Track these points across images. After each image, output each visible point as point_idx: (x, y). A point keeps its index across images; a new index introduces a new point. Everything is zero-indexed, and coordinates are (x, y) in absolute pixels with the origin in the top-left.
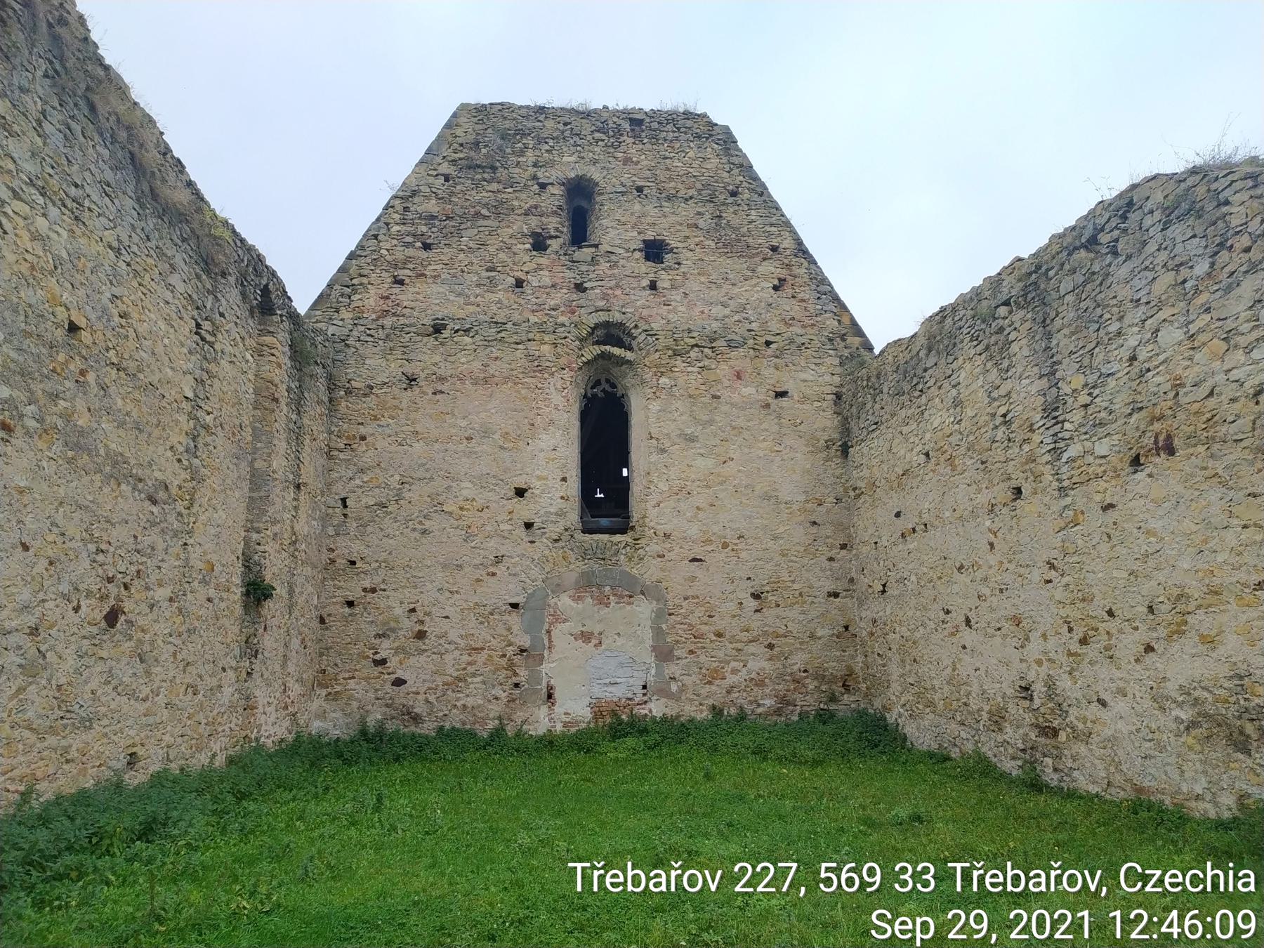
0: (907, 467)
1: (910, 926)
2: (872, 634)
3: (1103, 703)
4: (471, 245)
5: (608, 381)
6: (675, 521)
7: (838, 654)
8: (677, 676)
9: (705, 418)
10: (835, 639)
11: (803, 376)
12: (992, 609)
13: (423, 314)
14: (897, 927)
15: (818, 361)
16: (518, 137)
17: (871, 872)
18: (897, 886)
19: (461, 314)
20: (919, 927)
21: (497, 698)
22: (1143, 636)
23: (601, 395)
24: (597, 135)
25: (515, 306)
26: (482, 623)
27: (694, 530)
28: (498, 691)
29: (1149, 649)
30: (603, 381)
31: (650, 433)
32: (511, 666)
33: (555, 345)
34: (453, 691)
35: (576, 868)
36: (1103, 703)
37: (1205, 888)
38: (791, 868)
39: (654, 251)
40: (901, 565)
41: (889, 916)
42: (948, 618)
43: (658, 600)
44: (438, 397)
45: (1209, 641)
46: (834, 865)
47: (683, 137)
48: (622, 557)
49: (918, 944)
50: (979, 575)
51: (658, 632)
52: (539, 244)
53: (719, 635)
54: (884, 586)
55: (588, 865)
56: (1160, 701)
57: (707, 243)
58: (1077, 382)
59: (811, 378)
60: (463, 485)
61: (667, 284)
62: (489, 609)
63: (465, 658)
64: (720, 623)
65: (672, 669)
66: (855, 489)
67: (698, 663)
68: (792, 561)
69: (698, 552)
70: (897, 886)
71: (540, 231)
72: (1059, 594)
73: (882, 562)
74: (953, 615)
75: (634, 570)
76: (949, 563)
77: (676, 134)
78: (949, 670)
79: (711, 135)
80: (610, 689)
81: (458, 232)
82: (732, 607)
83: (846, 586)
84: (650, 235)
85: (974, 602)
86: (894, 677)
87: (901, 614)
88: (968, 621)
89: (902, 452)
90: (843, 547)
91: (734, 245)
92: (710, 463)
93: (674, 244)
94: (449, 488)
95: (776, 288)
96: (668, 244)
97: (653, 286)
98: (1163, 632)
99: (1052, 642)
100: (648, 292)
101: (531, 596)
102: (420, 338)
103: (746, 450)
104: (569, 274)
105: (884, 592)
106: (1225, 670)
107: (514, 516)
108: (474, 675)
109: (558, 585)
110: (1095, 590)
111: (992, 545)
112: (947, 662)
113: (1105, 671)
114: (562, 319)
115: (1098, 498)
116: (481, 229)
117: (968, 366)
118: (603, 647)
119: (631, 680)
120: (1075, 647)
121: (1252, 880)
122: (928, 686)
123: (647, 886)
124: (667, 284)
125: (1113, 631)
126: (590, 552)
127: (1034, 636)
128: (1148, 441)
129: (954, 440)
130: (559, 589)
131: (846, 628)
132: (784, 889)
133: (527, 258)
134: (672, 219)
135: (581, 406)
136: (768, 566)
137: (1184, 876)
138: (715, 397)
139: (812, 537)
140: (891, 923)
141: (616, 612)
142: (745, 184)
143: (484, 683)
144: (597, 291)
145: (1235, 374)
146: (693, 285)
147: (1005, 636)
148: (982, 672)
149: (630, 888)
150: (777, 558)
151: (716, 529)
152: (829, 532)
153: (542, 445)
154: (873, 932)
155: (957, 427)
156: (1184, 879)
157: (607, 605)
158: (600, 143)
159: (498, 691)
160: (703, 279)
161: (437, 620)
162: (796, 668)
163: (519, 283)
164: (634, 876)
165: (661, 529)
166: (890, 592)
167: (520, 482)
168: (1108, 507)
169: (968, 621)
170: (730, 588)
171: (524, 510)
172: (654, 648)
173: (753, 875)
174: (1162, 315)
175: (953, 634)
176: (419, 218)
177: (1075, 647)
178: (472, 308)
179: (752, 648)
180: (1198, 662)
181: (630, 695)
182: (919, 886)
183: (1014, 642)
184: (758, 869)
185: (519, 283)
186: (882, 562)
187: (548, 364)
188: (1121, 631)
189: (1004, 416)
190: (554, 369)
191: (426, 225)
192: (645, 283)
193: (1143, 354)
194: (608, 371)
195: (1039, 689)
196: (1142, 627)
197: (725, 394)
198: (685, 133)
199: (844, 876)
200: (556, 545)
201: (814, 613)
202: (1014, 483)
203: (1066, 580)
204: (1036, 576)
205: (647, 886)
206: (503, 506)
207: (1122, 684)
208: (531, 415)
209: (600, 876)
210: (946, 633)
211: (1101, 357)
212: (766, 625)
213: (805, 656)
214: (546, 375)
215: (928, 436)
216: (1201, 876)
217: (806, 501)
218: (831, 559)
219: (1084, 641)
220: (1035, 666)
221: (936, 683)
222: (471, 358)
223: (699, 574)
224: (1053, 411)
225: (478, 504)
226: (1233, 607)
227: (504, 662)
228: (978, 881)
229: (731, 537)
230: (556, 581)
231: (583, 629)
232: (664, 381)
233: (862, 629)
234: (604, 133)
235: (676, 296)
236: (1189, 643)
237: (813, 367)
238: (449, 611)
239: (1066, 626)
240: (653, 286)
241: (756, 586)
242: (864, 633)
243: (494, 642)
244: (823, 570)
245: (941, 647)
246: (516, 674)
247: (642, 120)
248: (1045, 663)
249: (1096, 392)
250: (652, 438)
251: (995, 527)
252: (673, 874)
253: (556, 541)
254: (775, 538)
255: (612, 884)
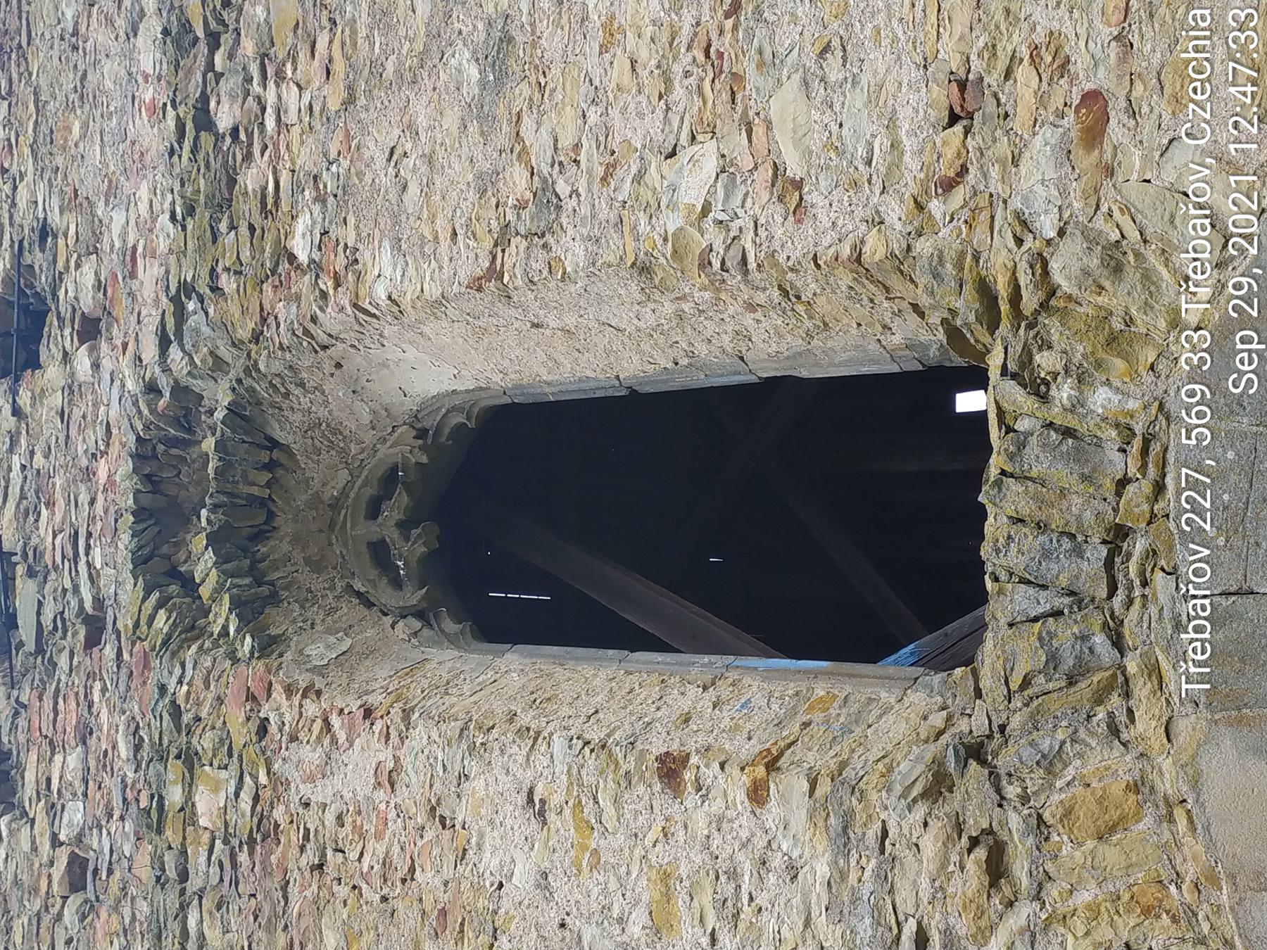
1: (1245, 355)
14: (1246, 368)
17: (1191, 394)
18: (1205, 368)
20: (1246, 347)
30: (372, 531)
31: (477, 285)
35: (1187, 690)
37: (1206, 59)
41: (1235, 376)
46: (1183, 431)
48: (1101, 398)
49: (1263, 347)
55: (1183, 677)
70: (1205, 368)
121: (1199, 12)
123: (1205, 618)
126: (1065, 632)
132: (1208, 481)
137: (1196, 80)
140: (1241, 374)
149: (1207, 635)
154: (1251, 392)
156: (1199, 80)
173: (1193, 512)
182: (1205, 346)
184: (1188, 507)
194: (335, 505)
199: (1195, 421)
200: (1020, 868)
205: (1205, 618)
209: (1195, 666)
216: (1194, 63)
228: (1200, 667)
250: (494, 273)
252: (1192, 212)
253: (996, 870)
255: (1203, 654)
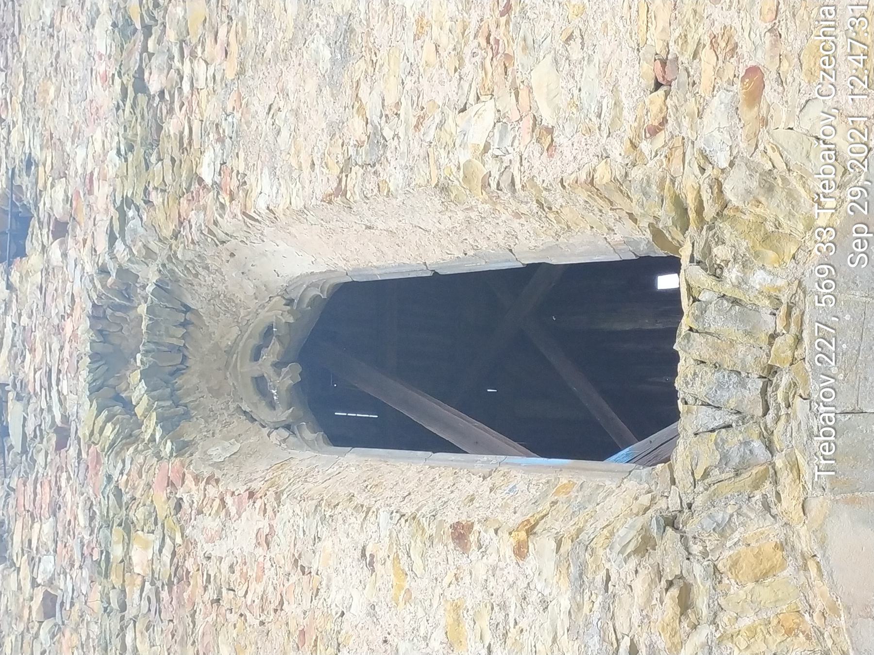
30: (256, 369)
31: (328, 199)
38: (818, 327)
48: (759, 278)
126: (733, 439)
135: (310, 445)
164: (825, 436)
194: (229, 352)
250: (340, 191)
253: (685, 603)
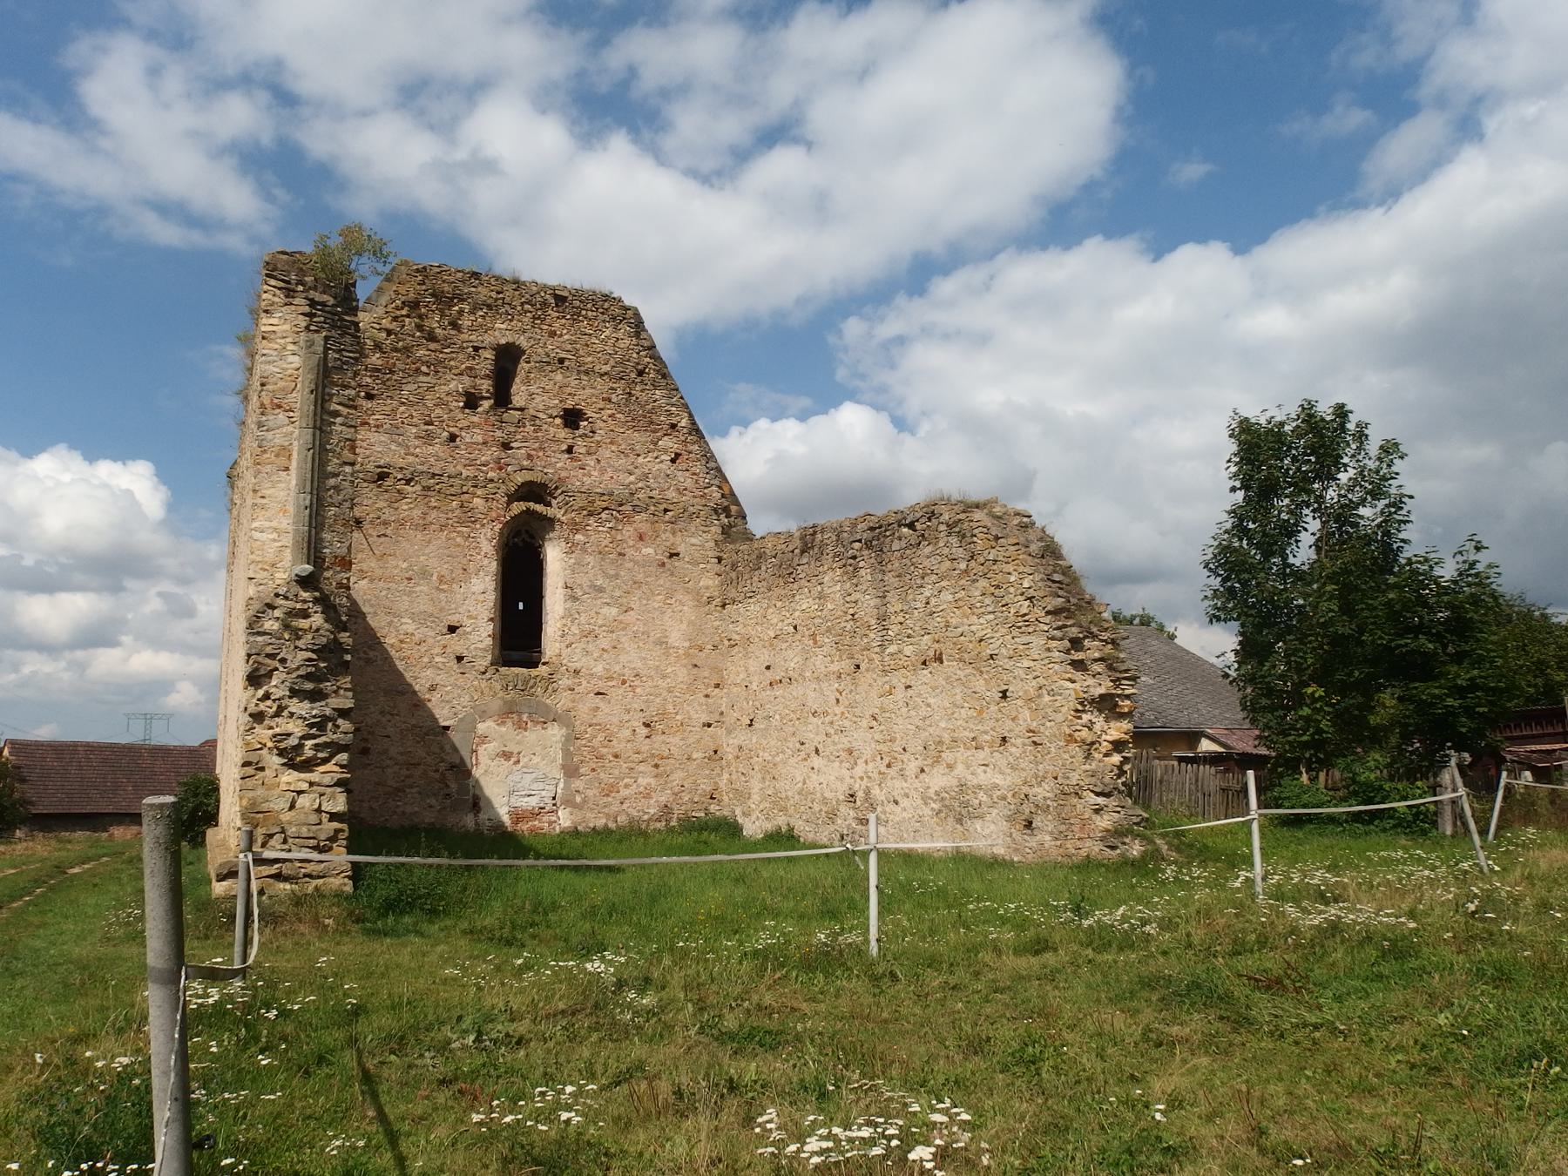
0: (778, 633)
2: (738, 757)
3: (896, 803)
4: (411, 399)
5: (527, 532)
6: (584, 659)
7: (707, 772)
8: (581, 789)
9: (612, 572)
10: (706, 760)
11: (694, 541)
12: (834, 743)
13: (367, 460)
15: (706, 529)
16: (455, 301)
19: (401, 463)
21: (431, 807)
22: (919, 763)
23: (521, 544)
24: (527, 307)
25: (450, 459)
26: (418, 742)
27: (599, 669)
28: (433, 801)
29: (922, 771)
32: (443, 780)
33: (487, 500)
34: (394, 800)
36: (896, 803)
39: (572, 418)
40: (768, 706)
42: (802, 747)
43: (567, 727)
44: (383, 539)
45: (950, 767)
47: (602, 317)
50: (828, 719)
51: (567, 754)
52: (471, 402)
53: (616, 756)
54: (751, 721)
56: (926, 800)
57: (618, 416)
58: (898, 607)
59: (699, 543)
60: (403, 620)
61: (583, 450)
62: (424, 730)
63: (404, 772)
64: (617, 746)
65: (578, 784)
66: (729, 640)
67: (599, 779)
68: (676, 697)
69: (601, 685)
71: (473, 391)
72: (878, 737)
73: (751, 703)
74: (807, 745)
75: (548, 701)
76: (806, 709)
77: (594, 314)
78: (800, 785)
79: (624, 319)
80: (526, 799)
81: (399, 385)
82: (627, 733)
83: (717, 718)
84: (570, 404)
85: (822, 738)
86: (756, 790)
87: (765, 742)
88: (817, 751)
89: (775, 620)
90: (717, 686)
91: (646, 421)
92: (614, 611)
93: (590, 414)
94: (390, 623)
95: (673, 461)
96: (586, 414)
97: (570, 450)
98: (930, 761)
99: (871, 765)
100: (567, 456)
101: (461, 720)
102: (365, 484)
103: (645, 602)
104: (498, 433)
105: (750, 725)
106: (955, 782)
107: (448, 650)
108: (411, 787)
109: (484, 711)
110: (897, 735)
111: (838, 700)
112: (799, 778)
113: (899, 783)
114: (491, 475)
115: (903, 680)
116: (420, 384)
117: (830, 574)
118: (521, 764)
119: (544, 793)
120: (883, 769)
122: (783, 796)
124: (583, 450)
125: (905, 760)
127: (860, 762)
128: (931, 653)
129: (817, 621)
130: (484, 715)
131: (716, 752)
133: (460, 416)
134: (588, 391)
136: (658, 700)
138: (620, 554)
139: (692, 677)
141: (533, 735)
142: (651, 366)
143: (420, 793)
144: (523, 451)
145: (973, 628)
146: (605, 453)
147: (842, 762)
148: (825, 785)
150: (665, 694)
151: (617, 668)
152: (706, 674)
153: (474, 589)
155: (820, 613)
157: (526, 730)
158: (528, 314)
159: (433, 801)
160: (613, 448)
161: (379, 738)
162: (675, 783)
163: (453, 438)
165: (573, 666)
166: (756, 725)
167: (453, 619)
168: (908, 687)
169: (817, 751)
170: (626, 717)
171: (456, 644)
172: (563, 767)
174: (943, 584)
175: (806, 759)
176: (366, 370)
177: (883, 769)
178: (411, 459)
179: (642, 767)
180: (945, 778)
181: (542, 805)
183: (847, 765)
185: (453, 438)
186: (751, 703)
187: (480, 516)
188: (909, 760)
189: (853, 615)
190: (485, 521)
191: (371, 376)
192: (564, 447)
193: (933, 601)
195: (860, 795)
196: (920, 759)
197: (630, 552)
198: (602, 313)
201: (691, 740)
202: (857, 662)
203: (882, 727)
204: (864, 723)
206: (439, 641)
207: (907, 791)
208: (464, 561)
210: (800, 758)
211: (911, 597)
212: (653, 749)
213: (683, 775)
214: (478, 526)
215: (797, 613)
217: (690, 647)
218: (707, 696)
219: (889, 766)
220: (859, 781)
221: (790, 794)
222: (412, 506)
223: (601, 705)
224: (882, 618)
225: (417, 638)
226: (962, 749)
227: (437, 776)
229: (628, 674)
230: (483, 708)
231: (505, 749)
232: (579, 537)
233: (729, 752)
234: (532, 305)
235: (591, 461)
236: (941, 768)
237: (700, 533)
238: (390, 730)
239: (879, 757)
240: (570, 450)
241: (647, 716)
242: (730, 757)
243: (429, 759)
244: (701, 705)
245: (796, 768)
246: (447, 786)
247: (567, 297)
248: (866, 779)
249: (907, 616)
251: (841, 688)
253: (484, 673)
254: (664, 677)
